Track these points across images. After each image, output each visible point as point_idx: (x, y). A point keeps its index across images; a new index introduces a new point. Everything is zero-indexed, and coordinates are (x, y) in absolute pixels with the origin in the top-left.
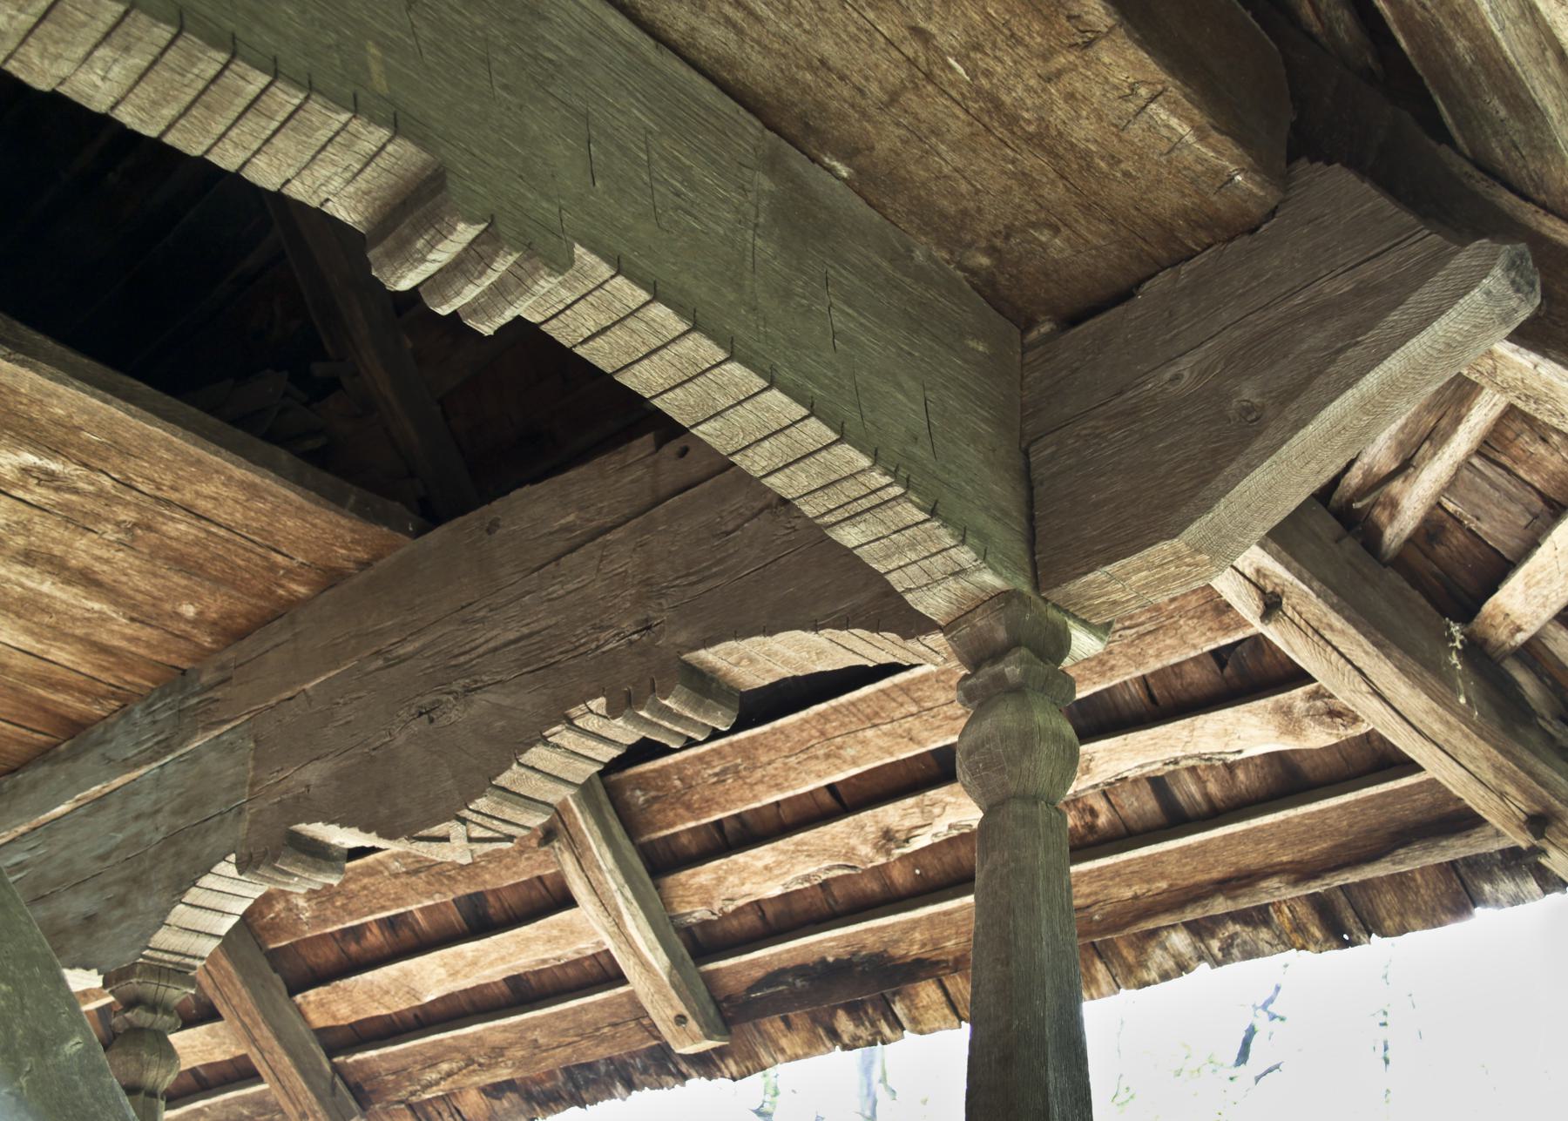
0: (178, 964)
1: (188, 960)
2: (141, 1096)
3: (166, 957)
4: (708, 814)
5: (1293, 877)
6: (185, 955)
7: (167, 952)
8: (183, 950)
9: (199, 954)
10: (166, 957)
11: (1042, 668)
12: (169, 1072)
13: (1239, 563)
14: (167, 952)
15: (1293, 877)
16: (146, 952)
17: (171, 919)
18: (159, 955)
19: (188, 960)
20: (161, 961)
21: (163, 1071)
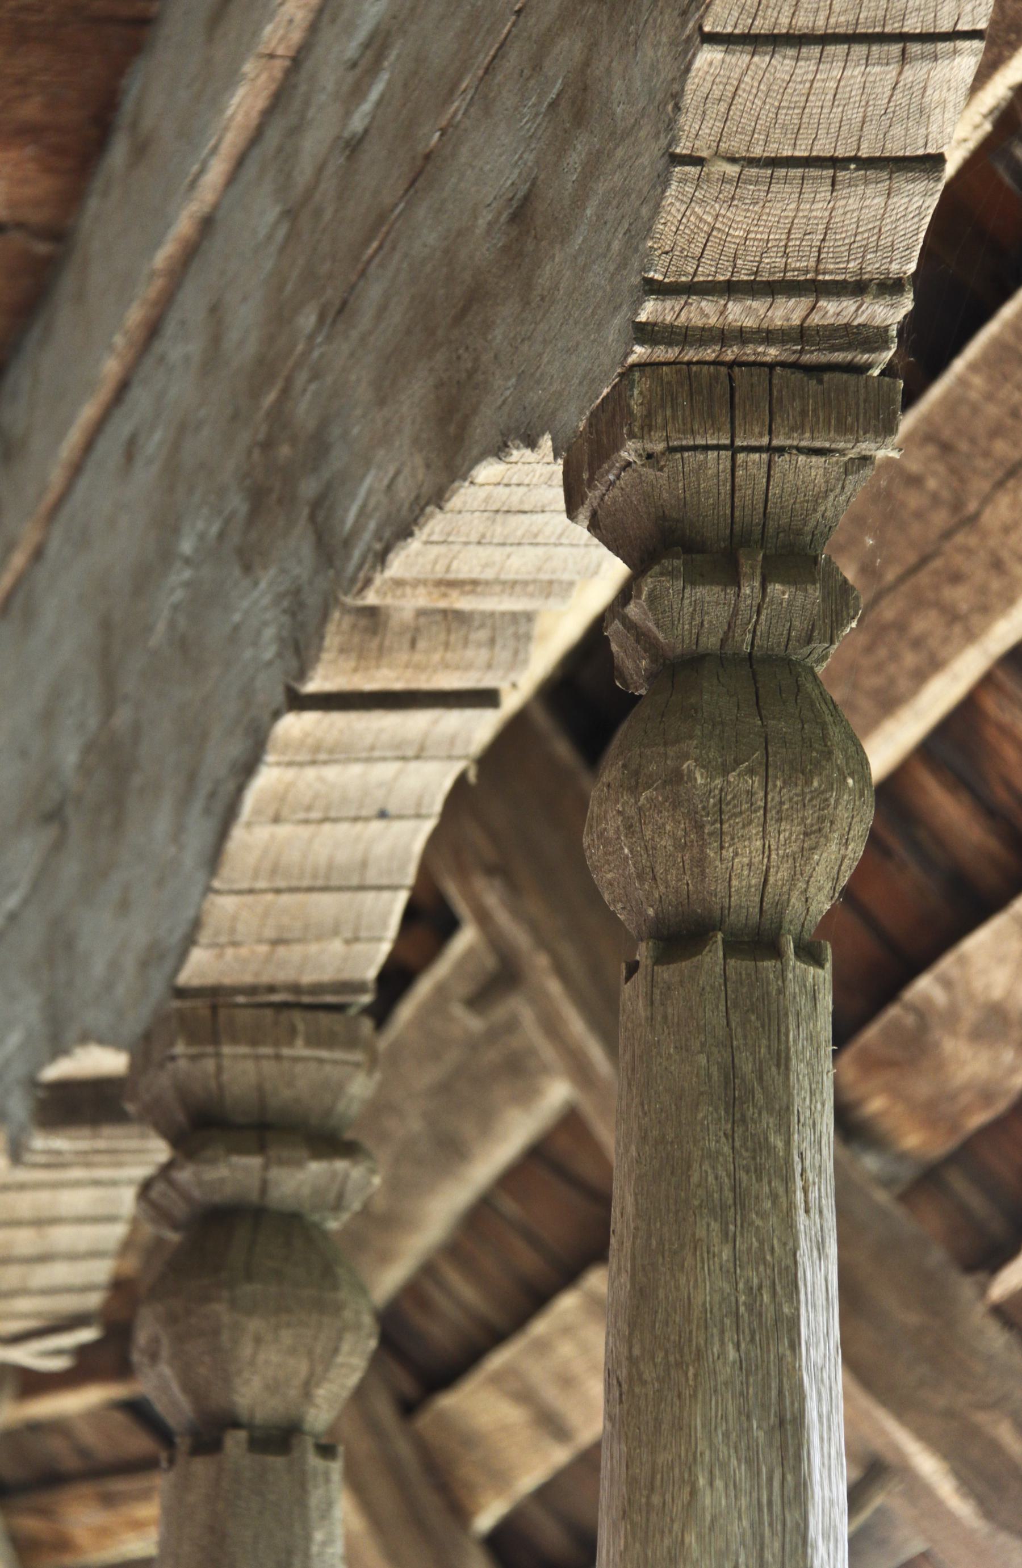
0: (802, 335)
1: (834, 311)
2: (713, 955)
3: (740, 313)
4: (601, 393)
5: (379, 568)
6: (818, 288)
7: (731, 289)
8: (800, 265)
9: (874, 266)
10: (740, 313)
11: (585, 359)
12: (815, 834)
13: (978, 45)
14: (731, 289)
15: (379, 568)
16: (649, 311)
17: (695, 133)
18: (703, 312)
19: (834, 311)
20: (723, 336)
21: (787, 835)
